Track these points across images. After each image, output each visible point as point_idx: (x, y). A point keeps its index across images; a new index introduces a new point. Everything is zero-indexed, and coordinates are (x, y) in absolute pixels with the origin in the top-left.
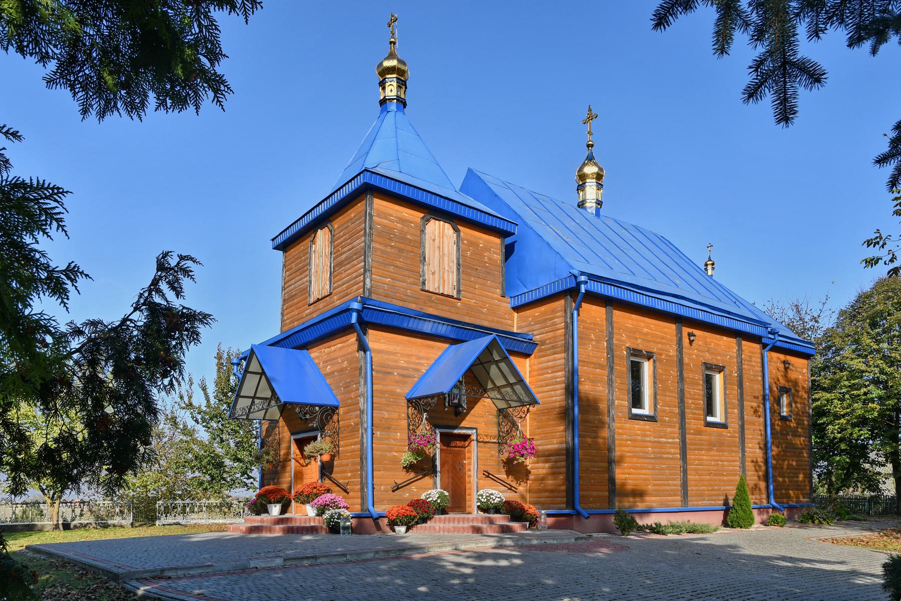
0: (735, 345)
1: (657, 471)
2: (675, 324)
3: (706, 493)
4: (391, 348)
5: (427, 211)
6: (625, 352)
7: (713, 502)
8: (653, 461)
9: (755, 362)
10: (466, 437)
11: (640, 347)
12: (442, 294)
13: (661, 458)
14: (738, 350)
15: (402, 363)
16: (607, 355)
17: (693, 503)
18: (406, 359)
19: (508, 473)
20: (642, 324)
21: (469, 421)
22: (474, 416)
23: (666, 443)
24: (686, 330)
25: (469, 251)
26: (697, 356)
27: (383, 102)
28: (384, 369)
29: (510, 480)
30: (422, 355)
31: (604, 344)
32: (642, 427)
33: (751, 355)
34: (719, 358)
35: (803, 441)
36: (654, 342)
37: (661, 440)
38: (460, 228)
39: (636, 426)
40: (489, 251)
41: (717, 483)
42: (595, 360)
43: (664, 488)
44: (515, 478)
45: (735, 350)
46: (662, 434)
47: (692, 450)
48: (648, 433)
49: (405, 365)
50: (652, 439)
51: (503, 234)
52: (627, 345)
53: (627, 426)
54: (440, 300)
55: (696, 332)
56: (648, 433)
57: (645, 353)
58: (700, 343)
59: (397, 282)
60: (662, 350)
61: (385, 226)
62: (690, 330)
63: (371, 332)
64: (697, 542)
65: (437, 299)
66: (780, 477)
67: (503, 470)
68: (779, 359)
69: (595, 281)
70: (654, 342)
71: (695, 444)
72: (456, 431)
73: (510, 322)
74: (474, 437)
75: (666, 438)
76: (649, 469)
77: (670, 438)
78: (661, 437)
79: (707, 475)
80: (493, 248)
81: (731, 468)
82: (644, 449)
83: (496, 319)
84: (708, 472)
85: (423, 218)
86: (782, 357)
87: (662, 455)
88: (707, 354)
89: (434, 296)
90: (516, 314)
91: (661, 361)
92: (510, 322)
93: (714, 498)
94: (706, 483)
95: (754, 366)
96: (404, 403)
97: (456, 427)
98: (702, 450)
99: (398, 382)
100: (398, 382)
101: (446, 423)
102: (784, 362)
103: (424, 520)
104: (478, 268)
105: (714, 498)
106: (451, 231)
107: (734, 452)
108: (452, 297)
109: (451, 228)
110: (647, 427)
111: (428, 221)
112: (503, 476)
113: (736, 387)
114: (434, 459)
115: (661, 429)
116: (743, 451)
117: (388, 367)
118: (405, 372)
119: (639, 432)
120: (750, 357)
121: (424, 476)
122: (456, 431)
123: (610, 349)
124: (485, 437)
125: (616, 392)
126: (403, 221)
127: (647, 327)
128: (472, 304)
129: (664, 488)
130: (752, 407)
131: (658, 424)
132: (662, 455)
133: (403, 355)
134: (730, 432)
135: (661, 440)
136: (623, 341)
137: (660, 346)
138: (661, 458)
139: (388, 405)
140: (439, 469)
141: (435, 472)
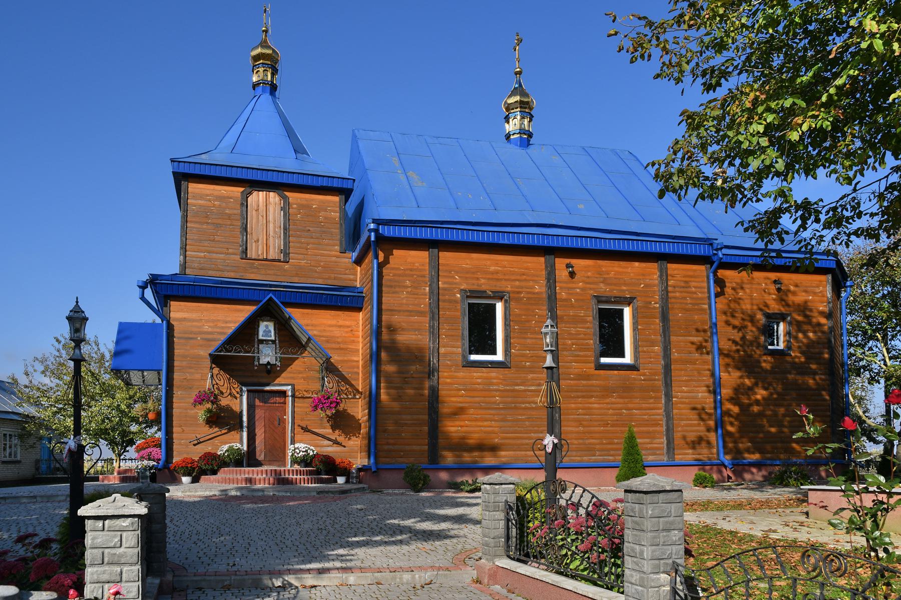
0: (656, 271)
1: (509, 423)
2: (544, 256)
3: (598, 447)
4: (194, 316)
5: (248, 185)
6: (459, 295)
7: (611, 458)
8: (502, 412)
9: (695, 287)
10: (283, 394)
11: (483, 288)
12: (266, 260)
13: (516, 408)
14: (661, 276)
15: (206, 328)
16: (430, 300)
17: (573, 458)
18: (211, 324)
19: (334, 428)
20: (489, 263)
21: (284, 378)
22: (290, 372)
23: (525, 391)
24: (561, 263)
25: (299, 214)
26: (583, 289)
27: (255, 86)
28: (186, 336)
29: (337, 435)
30: (229, 319)
31: (425, 289)
32: (485, 375)
33: (687, 279)
34: (625, 288)
35: (821, 379)
36: (506, 280)
37: (517, 388)
38: (287, 194)
39: (475, 374)
40: (326, 210)
41: (618, 435)
42: (411, 308)
43: (519, 442)
44: (343, 432)
45: (655, 277)
46: (519, 381)
47: (574, 397)
48: (495, 381)
49: (210, 330)
50: (501, 387)
51: (345, 193)
52: (462, 287)
53: (461, 374)
54: (263, 265)
55: (574, 262)
56: (495, 381)
57: (490, 293)
58: (589, 274)
59: (214, 255)
60: (522, 287)
61: (201, 206)
62: (567, 261)
63: (174, 304)
64: (462, 500)
65: (260, 265)
66: (771, 426)
67: (328, 424)
68: (768, 278)
69: (422, 226)
70: (506, 280)
71: (577, 391)
72: (268, 388)
73: (352, 277)
74: (290, 393)
75: (525, 386)
76: (495, 421)
77: (533, 386)
78: (519, 385)
79: (599, 426)
80: (329, 207)
81: (646, 417)
82: (487, 399)
83: (333, 276)
84: (602, 423)
85: (242, 192)
86: (773, 276)
87: (517, 405)
88: (602, 285)
89: (257, 263)
90: (359, 268)
91: (518, 300)
92: (352, 277)
93: (612, 452)
94: (597, 435)
95: (695, 293)
96: (208, 362)
97: (268, 385)
98: (592, 397)
99: (201, 346)
100: (201, 346)
101: (255, 380)
102: (775, 282)
103: (214, 472)
104: (311, 229)
105: (612, 452)
106: (277, 198)
107: (652, 398)
108: (279, 261)
109: (277, 195)
110: (494, 375)
111: (250, 193)
112: (328, 431)
113: (657, 321)
114: (241, 414)
115: (516, 375)
116: (669, 396)
117: (191, 333)
118: (210, 337)
119: (479, 381)
120: (686, 282)
121: (230, 430)
122: (268, 388)
123: (436, 293)
124: (305, 393)
125: (443, 338)
126: (221, 198)
127: (497, 265)
128: (302, 264)
129: (519, 442)
130: (692, 343)
131: (513, 370)
132: (517, 405)
133: (208, 321)
134: (644, 375)
135: (517, 388)
136: (456, 284)
137: (517, 283)
138: (516, 408)
139: (191, 368)
140: (245, 424)
141: (241, 427)
